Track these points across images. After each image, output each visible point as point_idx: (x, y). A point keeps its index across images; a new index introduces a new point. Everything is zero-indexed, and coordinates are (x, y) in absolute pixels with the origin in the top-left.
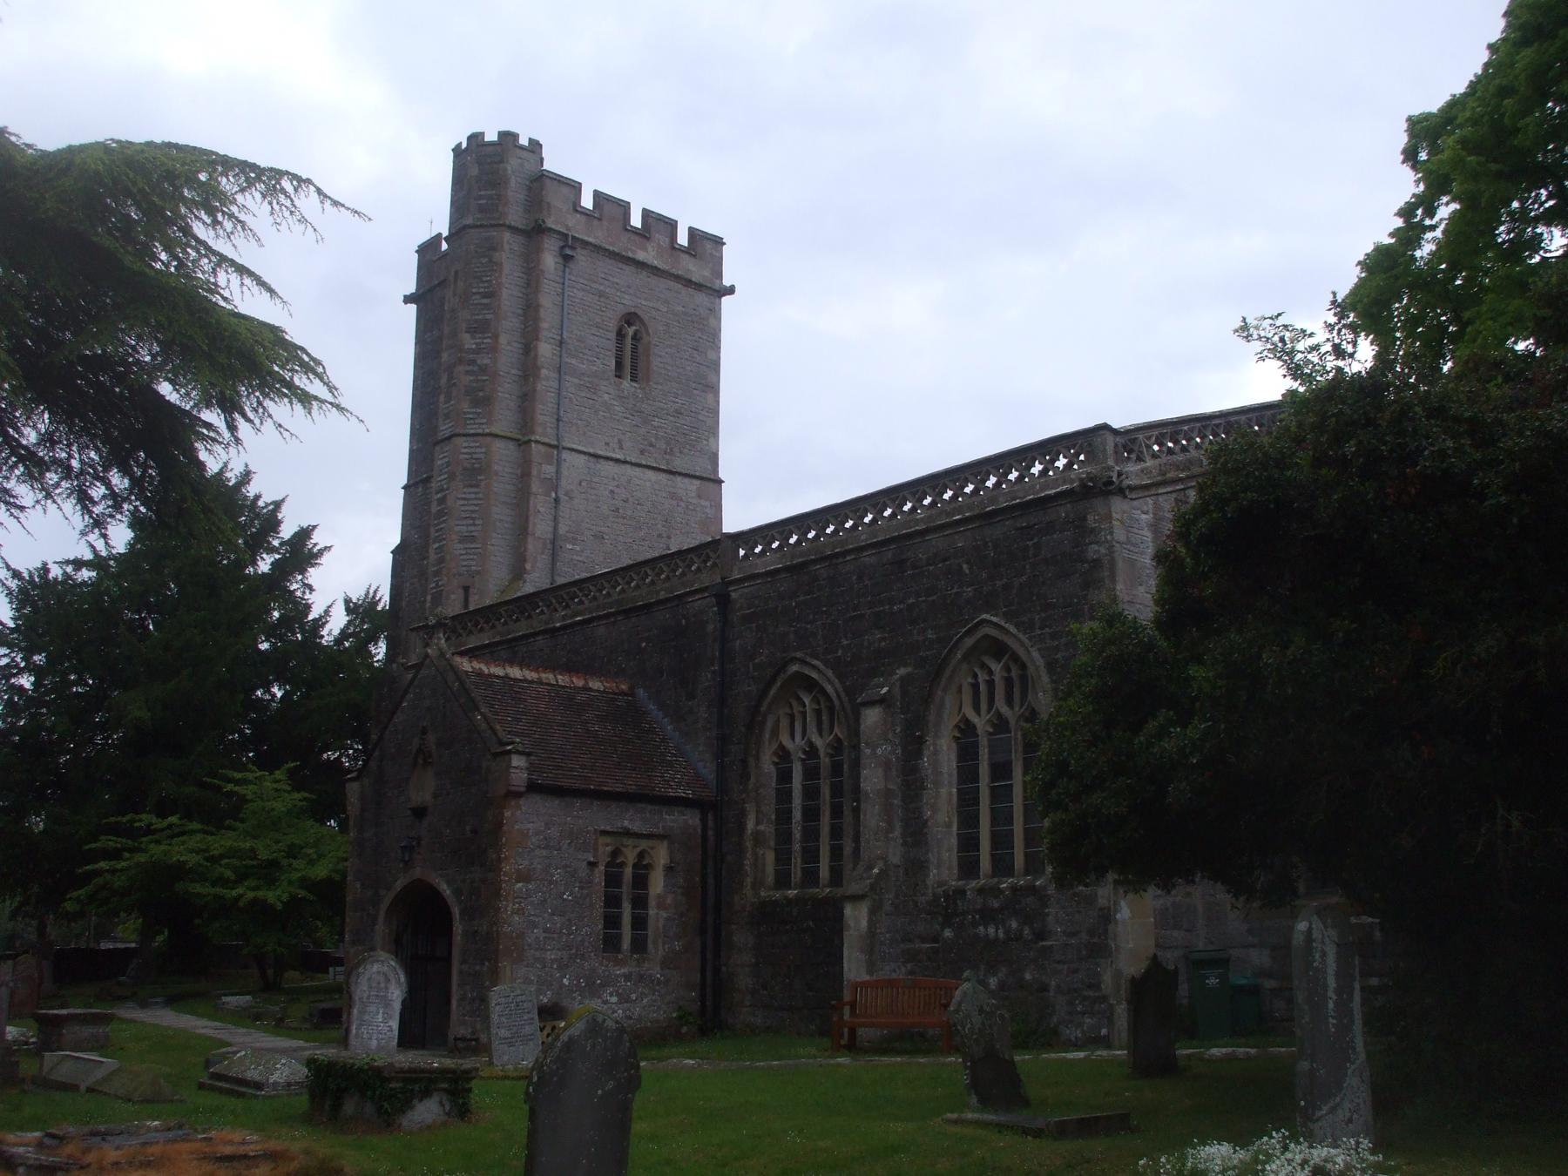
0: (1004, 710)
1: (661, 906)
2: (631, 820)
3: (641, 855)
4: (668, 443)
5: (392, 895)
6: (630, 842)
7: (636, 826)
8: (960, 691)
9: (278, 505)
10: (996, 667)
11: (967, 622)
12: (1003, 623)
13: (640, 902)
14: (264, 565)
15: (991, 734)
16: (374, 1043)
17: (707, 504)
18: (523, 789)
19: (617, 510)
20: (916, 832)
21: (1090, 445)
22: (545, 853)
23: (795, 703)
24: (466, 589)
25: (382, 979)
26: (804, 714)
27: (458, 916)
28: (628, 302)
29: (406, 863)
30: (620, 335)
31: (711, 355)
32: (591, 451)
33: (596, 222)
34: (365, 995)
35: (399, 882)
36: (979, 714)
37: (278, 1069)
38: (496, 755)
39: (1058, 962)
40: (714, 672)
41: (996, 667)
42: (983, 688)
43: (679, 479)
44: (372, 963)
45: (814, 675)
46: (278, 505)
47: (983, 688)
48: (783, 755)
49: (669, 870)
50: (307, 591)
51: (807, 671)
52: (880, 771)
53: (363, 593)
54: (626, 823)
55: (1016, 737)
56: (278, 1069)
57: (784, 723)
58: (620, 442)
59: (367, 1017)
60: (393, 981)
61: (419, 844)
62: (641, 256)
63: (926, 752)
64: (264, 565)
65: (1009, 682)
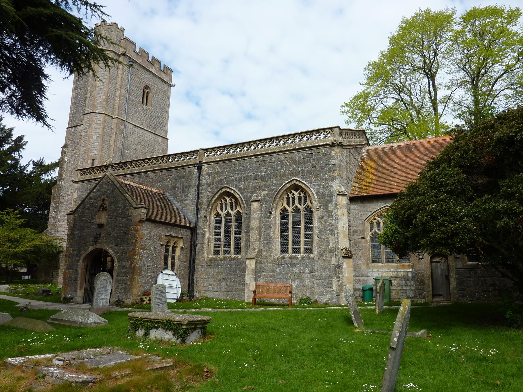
0: (230, 211)
1: (179, 259)
2: (173, 232)
3: (174, 243)
4: (155, 126)
5: (86, 253)
6: (172, 239)
7: (174, 234)
8: (283, 199)
9: (12, 129)
10: (296, 194)
11: (288, 179)
12: (301, 180)
13: (173, 258)
14: (7, 146)
15: (293, 212)
16: (102, 304)
17: (164, 145)
18: (144, 220)
19: (140, 143)
20: (268, 241)
21: (332, 132)
22: (149, 241)
23: (223, 200)
24: (93, 160)
25: (105, 282)
26: (226, 204)
27: (116, 261)
28: (147, 82)
29: (95, 242)
30: (144, 92)
31: (168, 103)
32: (134, 124)
33: (139, 56)
34: (99, 287)
35: (90, 249)
36: (289, 206)
37: (90, 317)
38: (135, 208)
39: (318, 280)
40: (195, 189)
41: (228, 199)
42: (291, 199)
43: (157, 136)
44: (102, 276)
45: (232, 192)
46: (12, 129)
47: (291, 199)
48: (218, 215)
49: (182, 248)
50: (21, 158)
51: (229, 190)
52: (258, 221)
53: (39, 160)
54: (171, 233)
55: (302, 214)
56: (90, 317)
57: (219, 206)
58: (142, 123)
59: (99, 295)
60: (108, 282)
61: (100, 237)
62: (151, 70)
63: (272, 217)
64: (7, 146)
65: (300, 198)
